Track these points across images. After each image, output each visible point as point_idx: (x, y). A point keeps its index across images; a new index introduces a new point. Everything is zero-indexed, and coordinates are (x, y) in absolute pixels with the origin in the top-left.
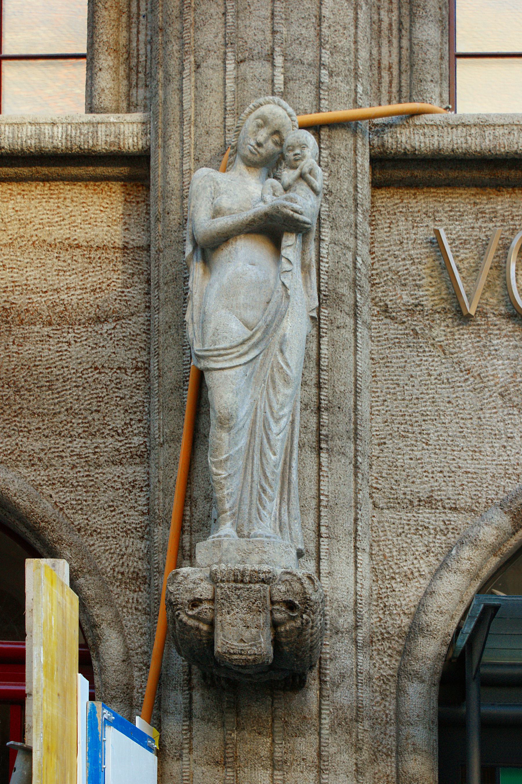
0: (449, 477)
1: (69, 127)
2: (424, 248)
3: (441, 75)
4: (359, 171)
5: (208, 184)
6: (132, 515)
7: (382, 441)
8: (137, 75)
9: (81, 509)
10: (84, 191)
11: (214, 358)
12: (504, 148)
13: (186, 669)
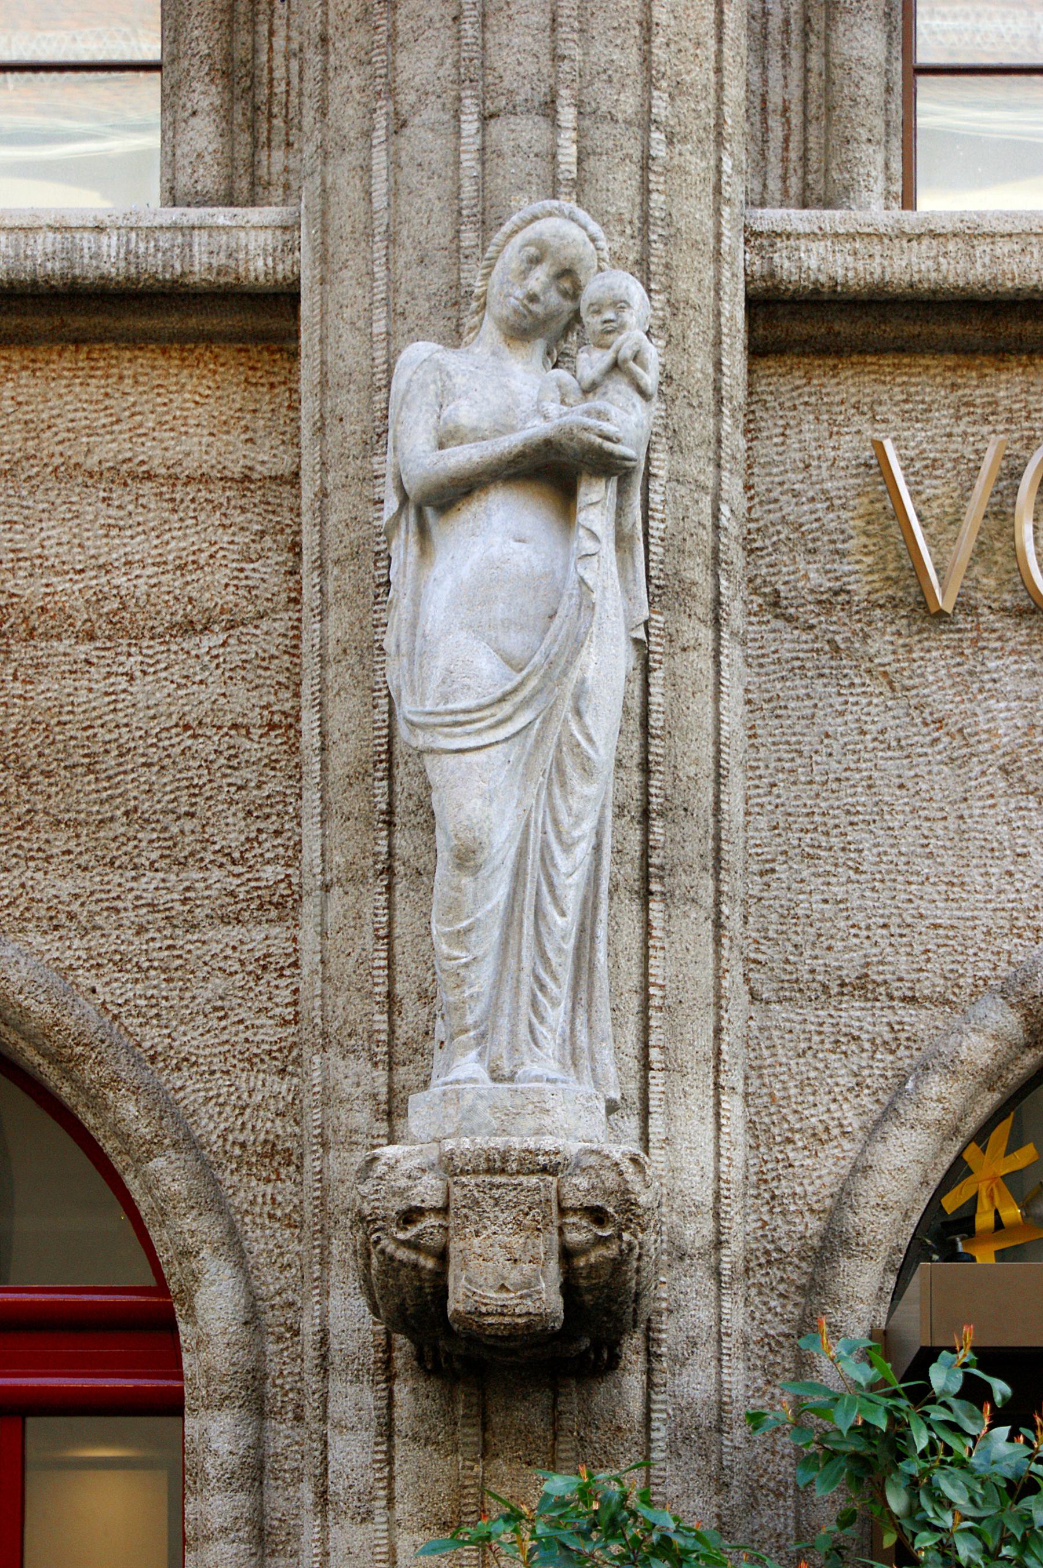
0: (901, 936)
1: (133, 235)
2: (853, 476)
3: (888, 124)
4: (725, 330)
5: (429, 378)
6: (262, 1026)
7: (768, 866)
8: (269, 122)
9: (157, 1015)
10: (161, 362)
11: (447, 730)
13: (382, 1339)
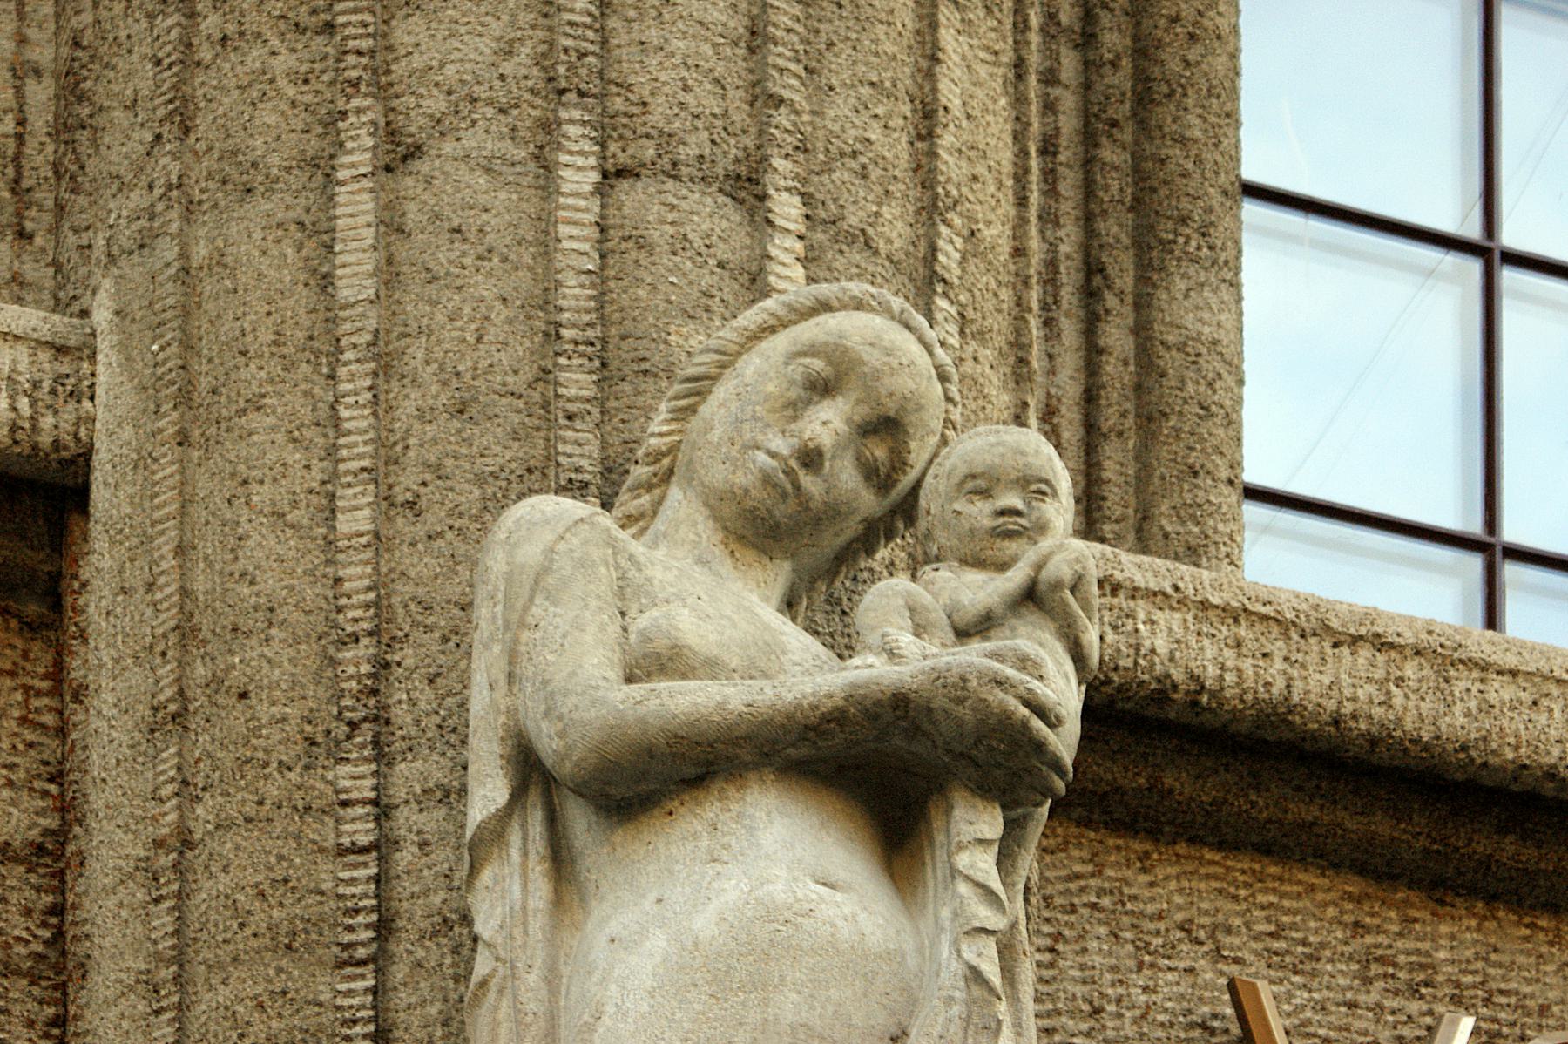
12: (1517, 748)
